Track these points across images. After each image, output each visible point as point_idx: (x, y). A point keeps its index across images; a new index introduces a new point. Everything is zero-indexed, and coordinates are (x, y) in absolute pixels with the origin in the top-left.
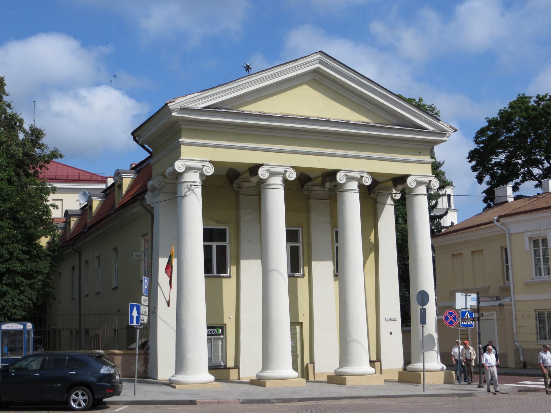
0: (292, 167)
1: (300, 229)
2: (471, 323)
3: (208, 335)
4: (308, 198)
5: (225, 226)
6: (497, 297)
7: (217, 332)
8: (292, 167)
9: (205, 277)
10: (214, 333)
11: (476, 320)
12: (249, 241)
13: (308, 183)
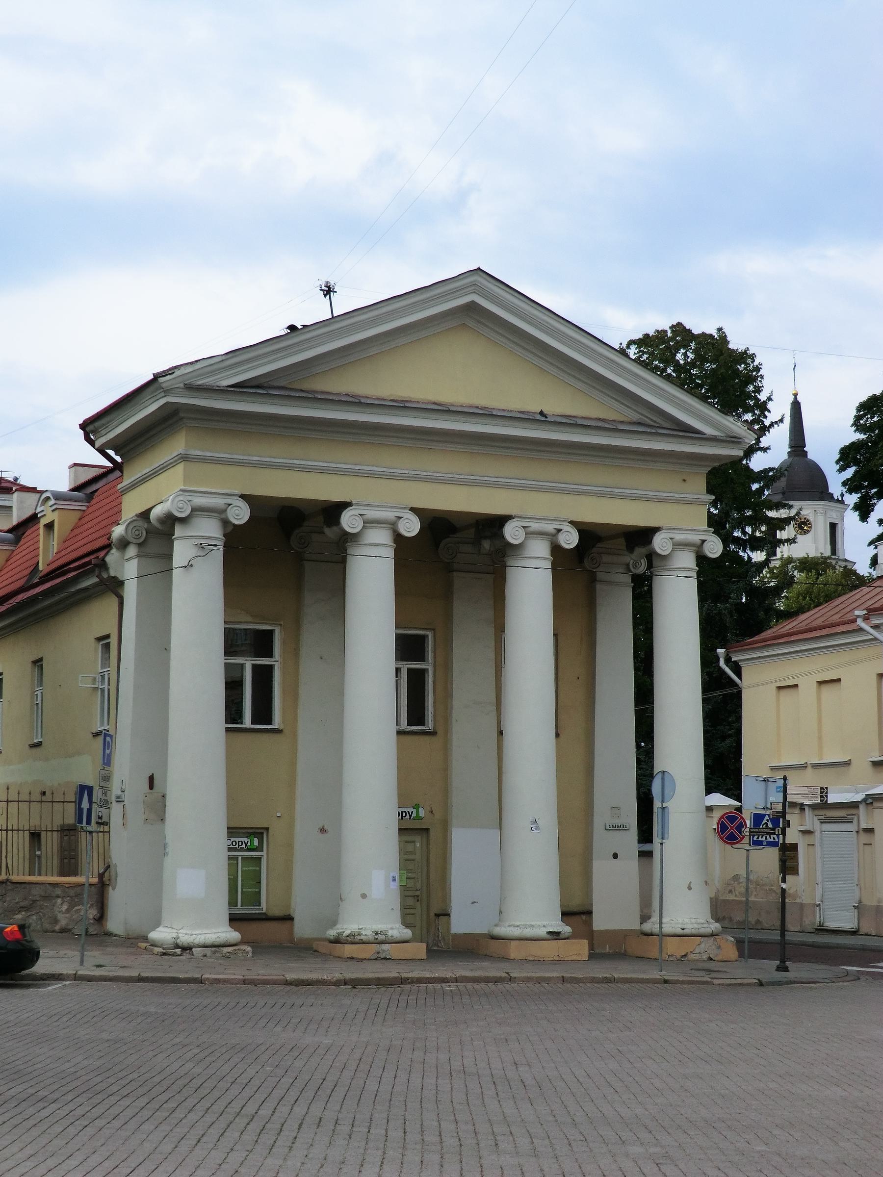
0: (412, 509)
1: (430, 634)
2: (774, 839)
3: (230, 849)
4: (449, 569)
5: (271, 624)
6: (822, 788)
7: (249, 844)
8: (412, 509)
9: (228, 730)
10: (244, 846)
11: (778, 833)
12: (321, 658)
13: (449, 537)
